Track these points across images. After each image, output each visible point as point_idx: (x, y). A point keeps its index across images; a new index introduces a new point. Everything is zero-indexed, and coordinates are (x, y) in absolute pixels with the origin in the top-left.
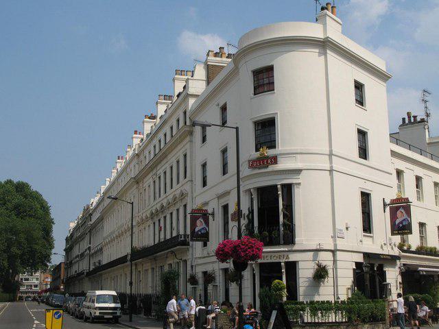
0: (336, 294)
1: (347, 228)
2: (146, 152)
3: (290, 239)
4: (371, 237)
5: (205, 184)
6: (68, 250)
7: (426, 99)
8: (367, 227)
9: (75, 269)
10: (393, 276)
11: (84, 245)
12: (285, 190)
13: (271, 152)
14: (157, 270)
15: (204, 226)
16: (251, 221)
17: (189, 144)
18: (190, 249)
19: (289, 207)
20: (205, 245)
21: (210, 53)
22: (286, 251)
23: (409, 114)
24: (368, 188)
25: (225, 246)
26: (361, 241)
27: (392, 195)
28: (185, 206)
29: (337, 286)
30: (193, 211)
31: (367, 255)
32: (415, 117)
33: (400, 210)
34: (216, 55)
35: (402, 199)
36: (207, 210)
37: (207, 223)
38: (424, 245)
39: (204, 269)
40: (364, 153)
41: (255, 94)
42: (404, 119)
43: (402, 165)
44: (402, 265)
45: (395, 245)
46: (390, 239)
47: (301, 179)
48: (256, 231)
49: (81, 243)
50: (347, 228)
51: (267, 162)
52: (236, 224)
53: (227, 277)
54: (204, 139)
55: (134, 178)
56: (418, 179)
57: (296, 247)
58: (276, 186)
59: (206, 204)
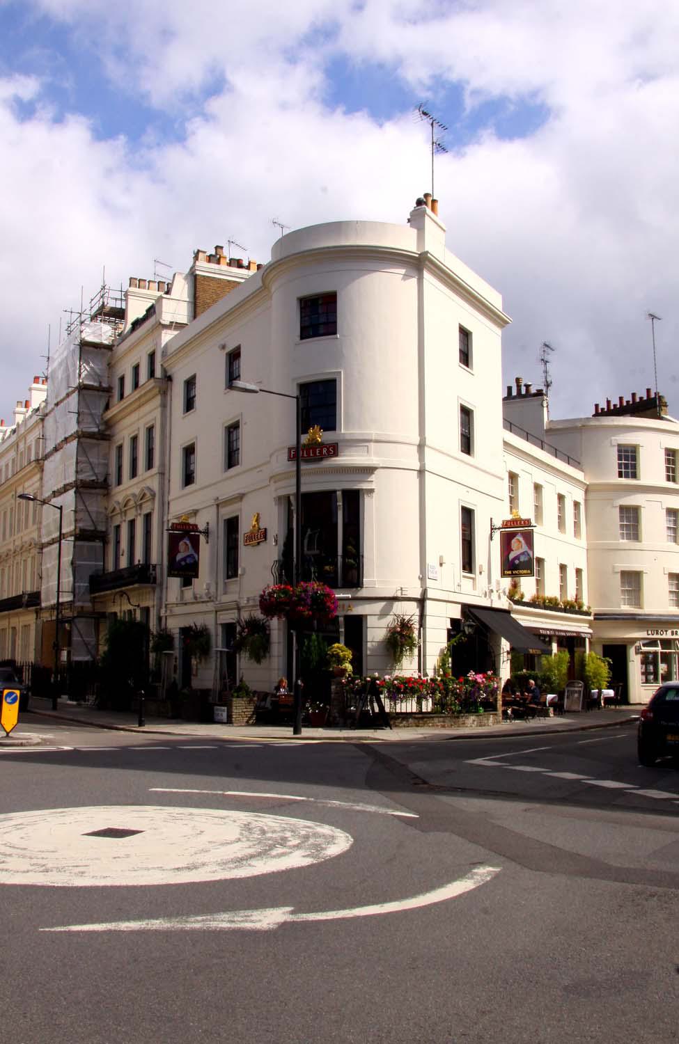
0: (421, 666)
1: (441, 565)
3: (353, 577)
5: (189, 479)
8: (468, 563)
13: (323, 437)
20: (187, 583)
21: (200, 254)
22: (347, 599)
29: (425, 656)
31: (467, 609)
32: (527, 386)
34: (210, 259)
35: (521, 520)
36: (196, 526)
38: (541, 595)
40: (467, 445)
42: (510, 389)
43: (517, 465)
45: (504, 593)
46: (498, 583)
47: (375, 481)
50: (441, 565)
51: (321, 452)
57: (363, 593)
58: (335, 492)
59: (195, 512)
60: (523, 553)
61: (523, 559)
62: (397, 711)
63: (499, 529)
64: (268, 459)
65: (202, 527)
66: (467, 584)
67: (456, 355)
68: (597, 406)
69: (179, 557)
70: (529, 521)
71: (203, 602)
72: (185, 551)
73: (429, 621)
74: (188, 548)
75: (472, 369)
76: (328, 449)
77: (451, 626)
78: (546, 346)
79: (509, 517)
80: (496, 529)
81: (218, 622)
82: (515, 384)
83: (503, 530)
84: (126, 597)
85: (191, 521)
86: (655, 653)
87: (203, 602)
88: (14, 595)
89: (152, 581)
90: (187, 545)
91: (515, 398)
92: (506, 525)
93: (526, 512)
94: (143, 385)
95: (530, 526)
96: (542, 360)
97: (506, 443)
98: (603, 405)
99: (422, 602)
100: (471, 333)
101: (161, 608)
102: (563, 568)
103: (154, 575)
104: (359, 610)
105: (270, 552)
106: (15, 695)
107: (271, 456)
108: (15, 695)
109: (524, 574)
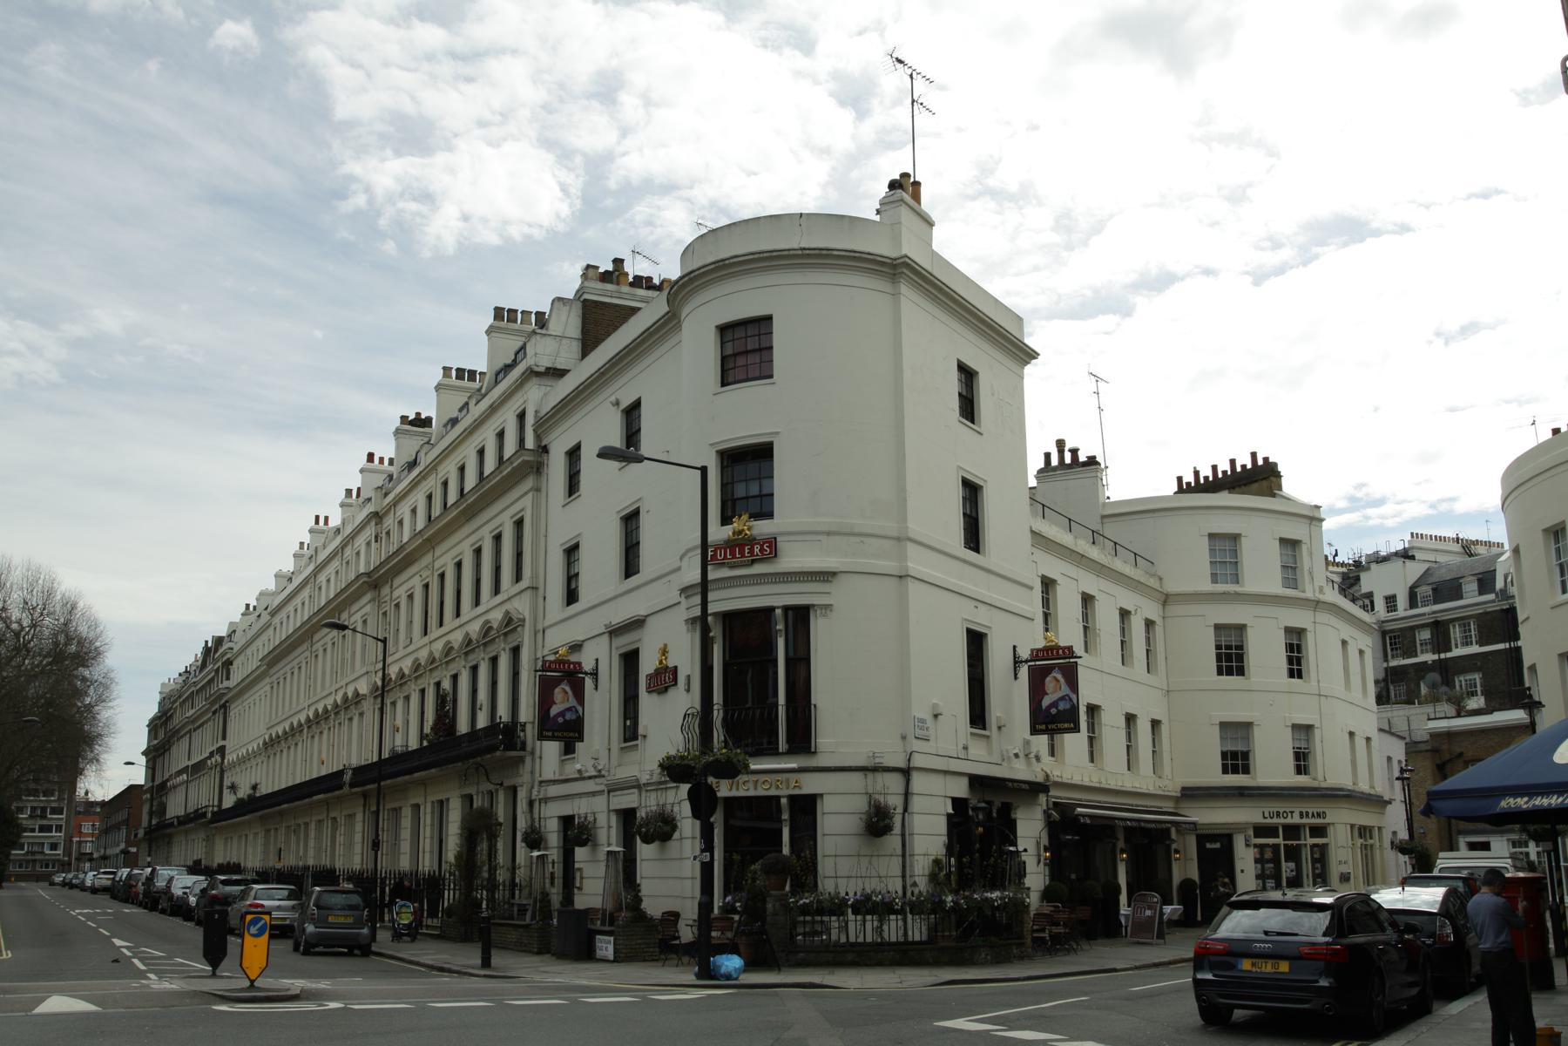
1: (936, 716)
2: (404, 510)
3: (802, 739)
4: (984, 736)
5: (571, 596)
6: (155, 754)
8: (978, 715)
9: (176, 807)
10: (1030, 830)
11: (200, 746)
13: (762, 528)
14: (429, 809)
15: (572, 702)
17: (529, 498)
18: (528, 760)
19: (800, 662)
20: (569, 749)
23: (1060, 444)
24: (982, 619)
25: (769, 743)
27: (1032, 638)
28: (516, 651)
31: (976, 782)
32: (1074, 452)
33: (1054, 674)
35: (1057, 648)
36: (579, 664)
39: (566, 809)
40: (973, 536)
41: (723, 384)
42: (1048, 456)
44: (1051, 806)
46: (1027, 743)
47: (836, 595)
49: (196, 736)
51: (751, 551)
55: (368, 574)
56: (1087, 599)
58: (771, 609)
59: (576, 647)
60: (1062, 698)
62: (852, 939)
63: (1026, 661)
64: (678, 564)
65: (588, 666)
66: (978, 750)
67: (955, 403)
68: (1180, 479)
70: (1070, 648)
71: (590, 778)
73: (917, 803)
74: (568, 700)
75: (980, 427)
76: (762, 546)
77: (953, 809)
79: (1041, 644)
80: (1021, 662)
81: (611, 808)
82: (1056, 449)
83: (1033, 663)
84: (484, 771)
85: (573, 658)
86: (1276, 847)
87: (590, 778)
88: (335, 770)
89: (519, 746)
90: (566, 693)
92: (1037, 655)
93: (1069, 633)
94: (509, 459)
97: (1035, 534)
98: (1189, 478)
99: (906, 772)
100: (977, 373)
101: (532, 787)
102: (1130, 719)
103: (523, 738)
104: (810, 785)
105: (683, 700)
106: (263, 922)
107: (681, 559)
108: (263, 922)
109: (1068, 729)
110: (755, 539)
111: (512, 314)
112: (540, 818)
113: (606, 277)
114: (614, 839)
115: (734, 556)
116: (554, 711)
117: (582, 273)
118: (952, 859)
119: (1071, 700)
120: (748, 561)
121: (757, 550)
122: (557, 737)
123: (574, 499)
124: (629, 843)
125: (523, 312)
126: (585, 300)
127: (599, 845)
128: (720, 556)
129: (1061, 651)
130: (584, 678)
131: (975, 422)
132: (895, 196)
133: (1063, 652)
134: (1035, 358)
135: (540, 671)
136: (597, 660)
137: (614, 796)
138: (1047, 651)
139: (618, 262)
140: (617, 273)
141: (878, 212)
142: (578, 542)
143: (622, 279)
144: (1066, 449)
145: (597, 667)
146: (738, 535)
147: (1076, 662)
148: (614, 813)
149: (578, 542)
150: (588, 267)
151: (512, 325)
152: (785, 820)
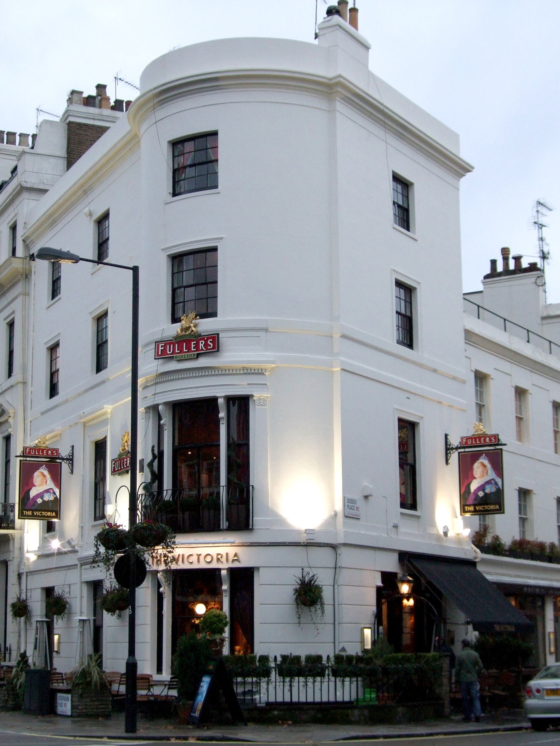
5: (53, 390)
7: (542, 220)
12: (234, 410)
16: (158, 476)
23: (505, 252)
26: (396, 527)
30: (27, 452)
32: (517, 259)
35: (485, 436)
36: (57, 450)
37: (57, 478)
41: (174, 194)
42: (494, 263)
48: (406, 639)
52: (126, 480)
53: (99, 601)
54: (55, 291)
58: (214, 400)
61: (48, 497)
63: (457, 448)
65: (64, 452)
67: (389, 212)
69: (474, 486)
72: (482, 476)
74: (46, 482)
75: (414, 233)
76: (206, 341)
77: (383, 582)
78: (539, 203)
80: (452, 449)
81: (83, 580)
83: (462, 450)
90: (45, 476)
91: (500, 274)
92: (466, 443)
95: (498, 445)
96: (535, 223)
110: (200, 335)
111: (11, 137)
112: (27, 590)
113: (89, 101)
114: (85, 609)
115: (181, 351)
116: (33, 493)
117: (67, 98)
118: (381, 628)
119: (496, 484)
120: (194, 355)
121: (201, 345)
122: (37, 516)
123: (56, 301)
124: (96, 612)
125: (21, 135)
126: (70, 122)
127: (72, 613)
128: (170, 351)
129: (487, 439)
130: (61, 463)
131: (411, 229)
132: (332, 21)
133: (490, 440)
134: (469, 171)
135: (21, 456)
136: (73, 447)
137: (85, 569)
138: (39, 450)
139: (101, 88)
140: (99, 98)
141: (316, 36)
142: (59, 340)
143: (104, 102)
144: (511, 256)
145: (73, 453)
146: (186, 332)
147: (501, 449)
148: (85, 584)
149: (59, 340)
150: (73, 92)
151: (11, 147)
152: (225, 591)
